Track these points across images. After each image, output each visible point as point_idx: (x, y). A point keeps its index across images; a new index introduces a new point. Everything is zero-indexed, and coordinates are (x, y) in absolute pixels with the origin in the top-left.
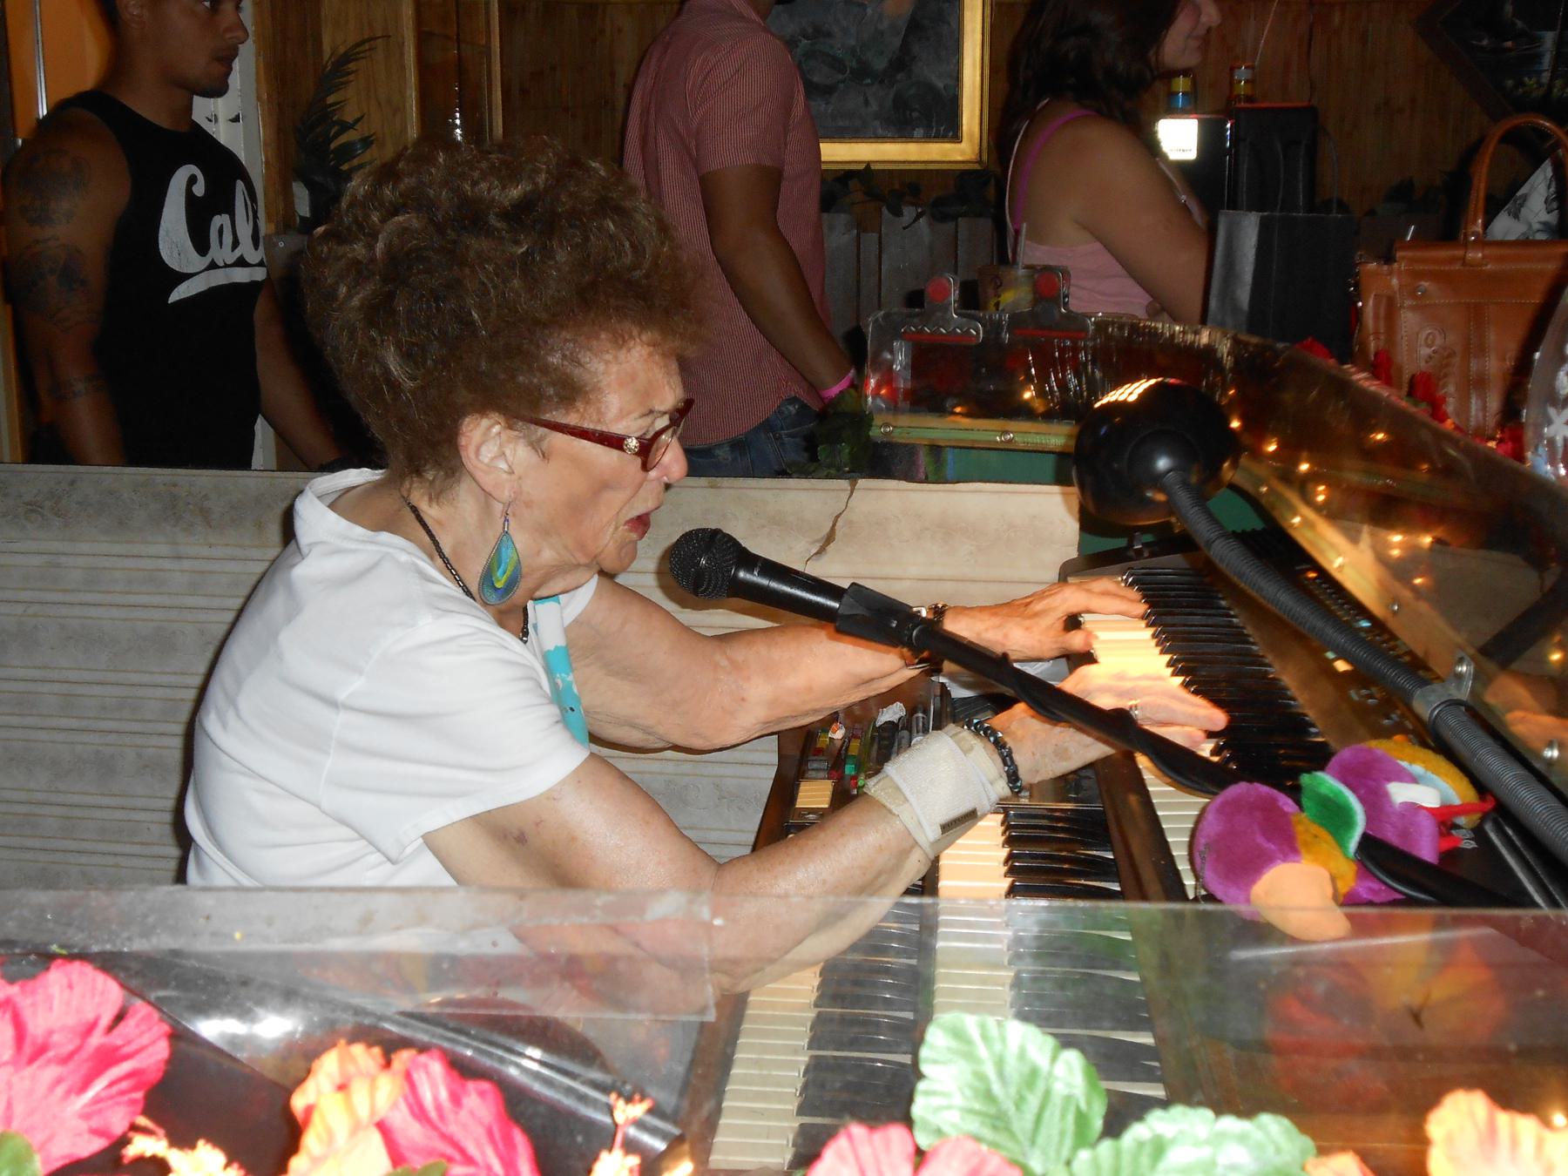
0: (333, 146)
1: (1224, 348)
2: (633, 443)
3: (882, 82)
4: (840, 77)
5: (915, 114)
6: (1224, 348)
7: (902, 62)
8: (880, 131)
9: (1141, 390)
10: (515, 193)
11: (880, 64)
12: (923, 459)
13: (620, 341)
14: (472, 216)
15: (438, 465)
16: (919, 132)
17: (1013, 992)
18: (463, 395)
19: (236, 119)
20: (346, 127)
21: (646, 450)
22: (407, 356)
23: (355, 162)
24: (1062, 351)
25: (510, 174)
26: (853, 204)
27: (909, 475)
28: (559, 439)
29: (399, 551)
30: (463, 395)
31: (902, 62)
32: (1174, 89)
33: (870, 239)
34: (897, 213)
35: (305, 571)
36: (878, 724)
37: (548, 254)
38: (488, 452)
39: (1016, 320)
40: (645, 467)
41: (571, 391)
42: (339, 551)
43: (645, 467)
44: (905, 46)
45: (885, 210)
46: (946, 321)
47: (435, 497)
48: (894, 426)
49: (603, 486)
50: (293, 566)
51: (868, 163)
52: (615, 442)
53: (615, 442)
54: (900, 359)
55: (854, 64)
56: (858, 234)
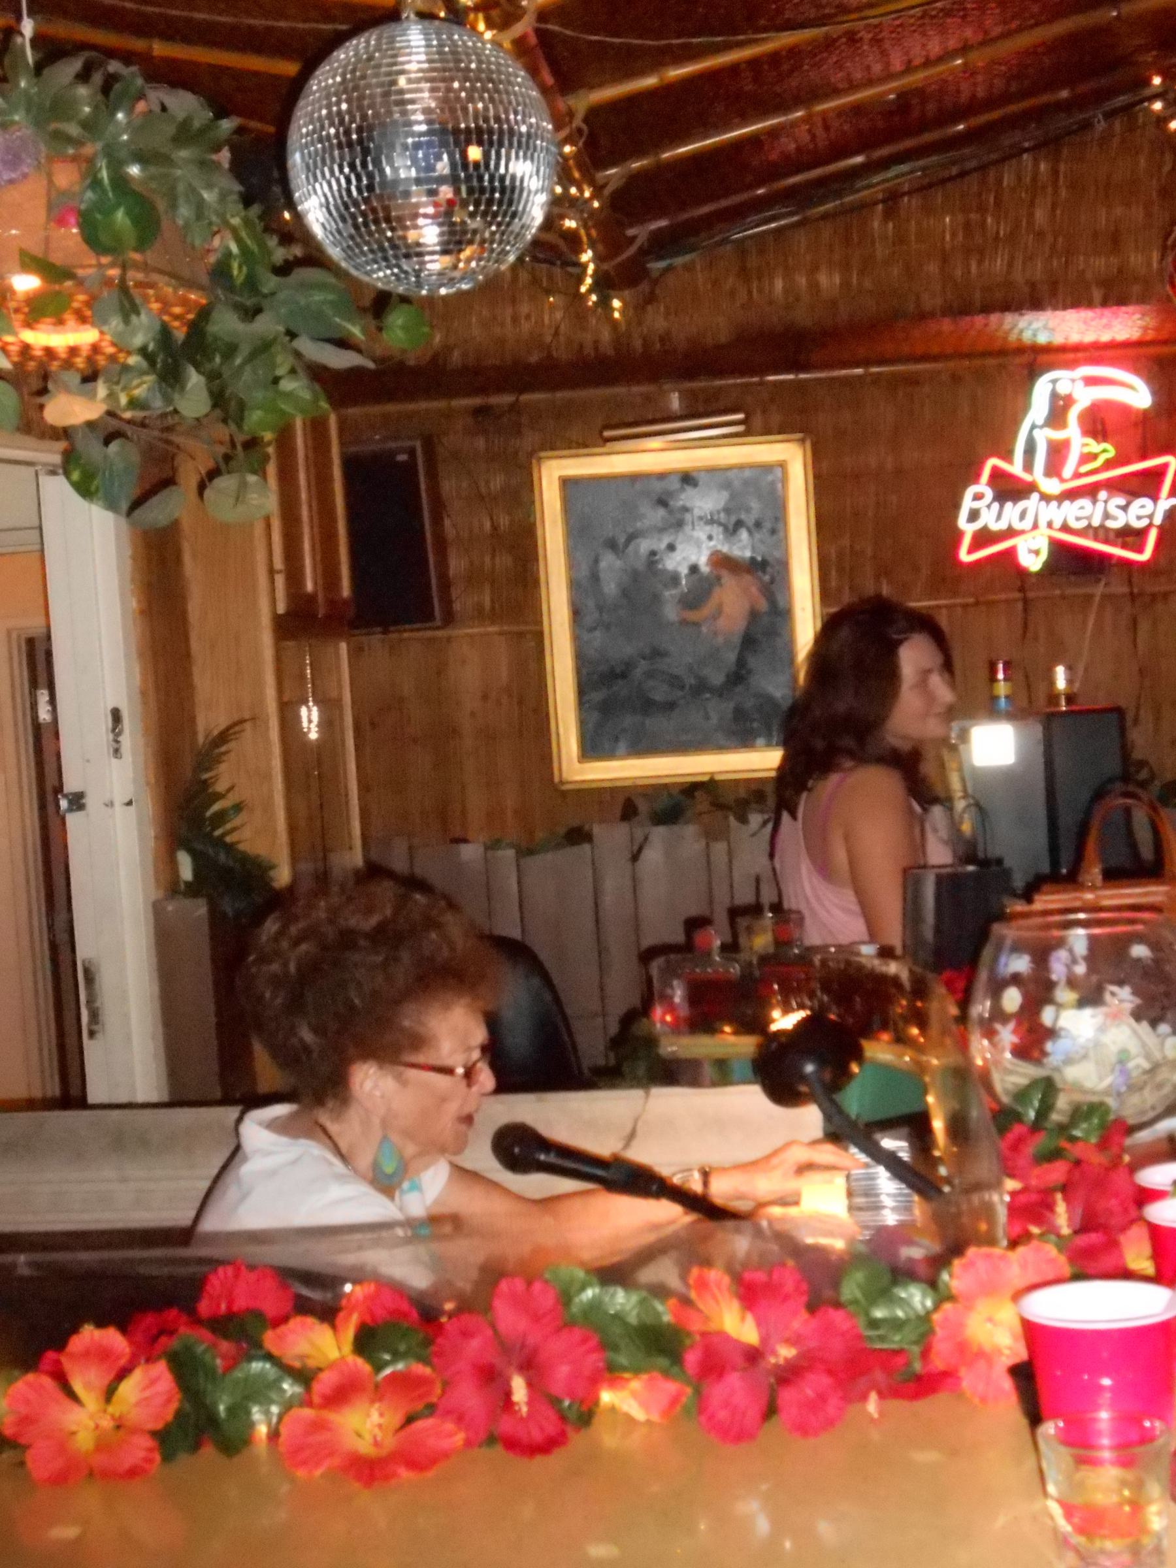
0: (208, 814)
1: (905, 976)
2: (460, 1071)
3: (721, 696)
4: (680, 693)
5: (755, 725)
6: (905, 976)
7: (739, 676)
8: (722, 742)
9: (799, 1018)
10: (374, 920)
11: (717, 678)
12: (708, 1071)
13: (447, 1007)
14: (348, 939)
15: (335, 1096)
16: (760, 741)
17: (84, 801)
18: (352, 1051)
19: (129, 803)
20: (219, 796)
21: (469, 1074)
22: (315, 1030)
23: (228, 826)
24: (798, 981)
25: (369, 911)
26: (700, 814)
27: (695, 1082)
28: (413, 1073)
29: (312, 1150)
30: (352, 1051)
31: (739, 676)
32: (996, 692)
33: (720, 848)
34: (743, 820)
35: (248, 1169)
36: (876, 1416)
37: (397, 960)
38: (368, 1085)
39: (764, 959)
40: (469, 1085)
41: (418, 1042)
42: (269, 1153)
43: (469, 1085)
44: (741, 662)
45: (732, 818)
46: (710, 962)
47: (338, 1116)
48: (674, 1046)
49: (444, 1099)
50: (239, 1167)
51: (712, 774)
52: (448, 1071)
53: (448, 1071)
54: (678, 995)
55: (693, 682)
56: (708, 845)
